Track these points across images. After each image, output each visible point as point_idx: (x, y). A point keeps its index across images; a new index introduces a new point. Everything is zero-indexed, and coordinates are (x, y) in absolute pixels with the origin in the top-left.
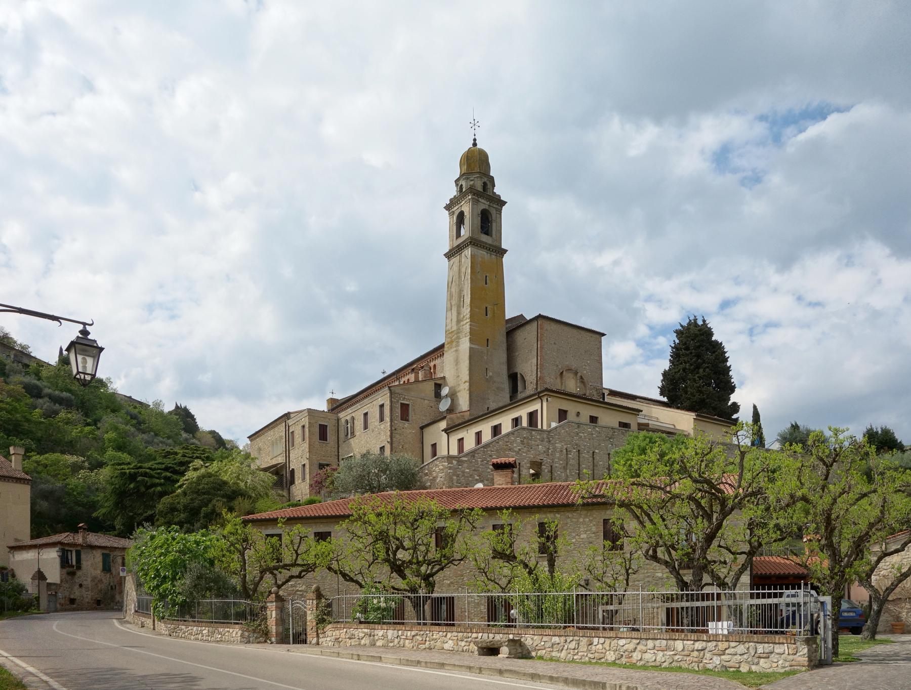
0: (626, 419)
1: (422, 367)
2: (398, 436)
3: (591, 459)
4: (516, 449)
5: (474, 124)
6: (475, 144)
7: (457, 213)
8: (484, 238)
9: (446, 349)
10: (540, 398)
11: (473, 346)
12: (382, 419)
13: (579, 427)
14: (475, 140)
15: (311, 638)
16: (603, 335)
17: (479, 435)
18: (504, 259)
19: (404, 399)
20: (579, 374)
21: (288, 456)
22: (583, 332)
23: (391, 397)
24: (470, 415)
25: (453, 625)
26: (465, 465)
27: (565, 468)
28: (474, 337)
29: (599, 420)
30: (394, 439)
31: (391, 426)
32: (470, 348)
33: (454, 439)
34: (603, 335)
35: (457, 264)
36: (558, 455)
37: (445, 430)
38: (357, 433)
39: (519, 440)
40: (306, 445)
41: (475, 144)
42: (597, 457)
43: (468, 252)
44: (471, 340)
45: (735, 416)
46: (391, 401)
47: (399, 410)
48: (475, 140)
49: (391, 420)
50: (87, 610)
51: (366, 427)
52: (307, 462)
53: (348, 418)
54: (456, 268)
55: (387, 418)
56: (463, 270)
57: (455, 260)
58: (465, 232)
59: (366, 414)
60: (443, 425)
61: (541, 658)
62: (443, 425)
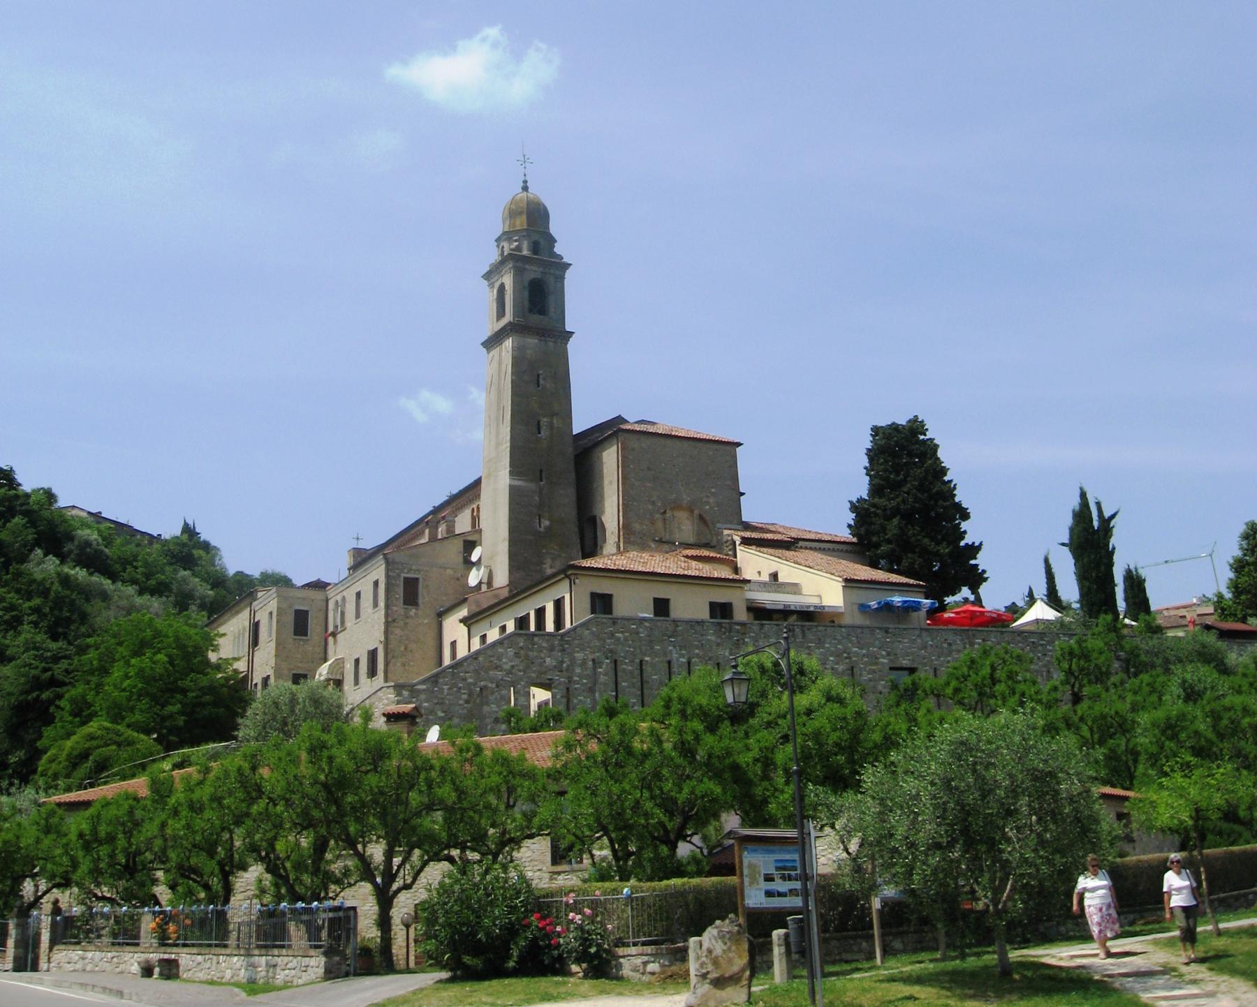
0: (721, 596)
1: (443, 518)
2: (398, 631)
3: (637, 672)
4: (507, 667)
5: (525, 161)
6: (525, 188)
7: (497, 285)
8: (535, 319)
9: (483, 485)
10: (567, 576)
11: (517, 483)
12: (376, 605)
13: (614, 623)
14: (525, 182)
15: (43, 965)
16: (739, 444)
17: (503, 628)
18: (569, 346)
19: (409, 571)
20: (696, 512)
21: (251, 662)
22: (699, 444)
23: (387, 570)
24: (510, 591)
25: (138, 945)
26: (423, 697)
27: (591, 690)
28: (517, 468)
29: (672, 606)
30: (392, 637)
31: (387, 615)
32: (512, 488)
33: (478, 630)
34: (739, 444)
35: (496, 358)
36: (578, 670)
37: (463, 621)
38: (348, 624)
39: (511, 652)
40: (273, 645)
41: (525, 188)
42: (648, 669)
43: (508, 343)
44: (511, 473)
45: (973, 562)
46: (388, 577)
47: (400, 590)
48: (525, 182)
49: (387, 607)
50: (356, 974)
51: (358, 616)
52: (271, 672)
53: (339, 598)
54: (495, 364)
55: (382, 604)
56: (504, 366)
57: (495, 352)
58: (508, 317)
59: (358, 595)
60: (464, 612)
61: (287, 985)
62: (464, 612)
